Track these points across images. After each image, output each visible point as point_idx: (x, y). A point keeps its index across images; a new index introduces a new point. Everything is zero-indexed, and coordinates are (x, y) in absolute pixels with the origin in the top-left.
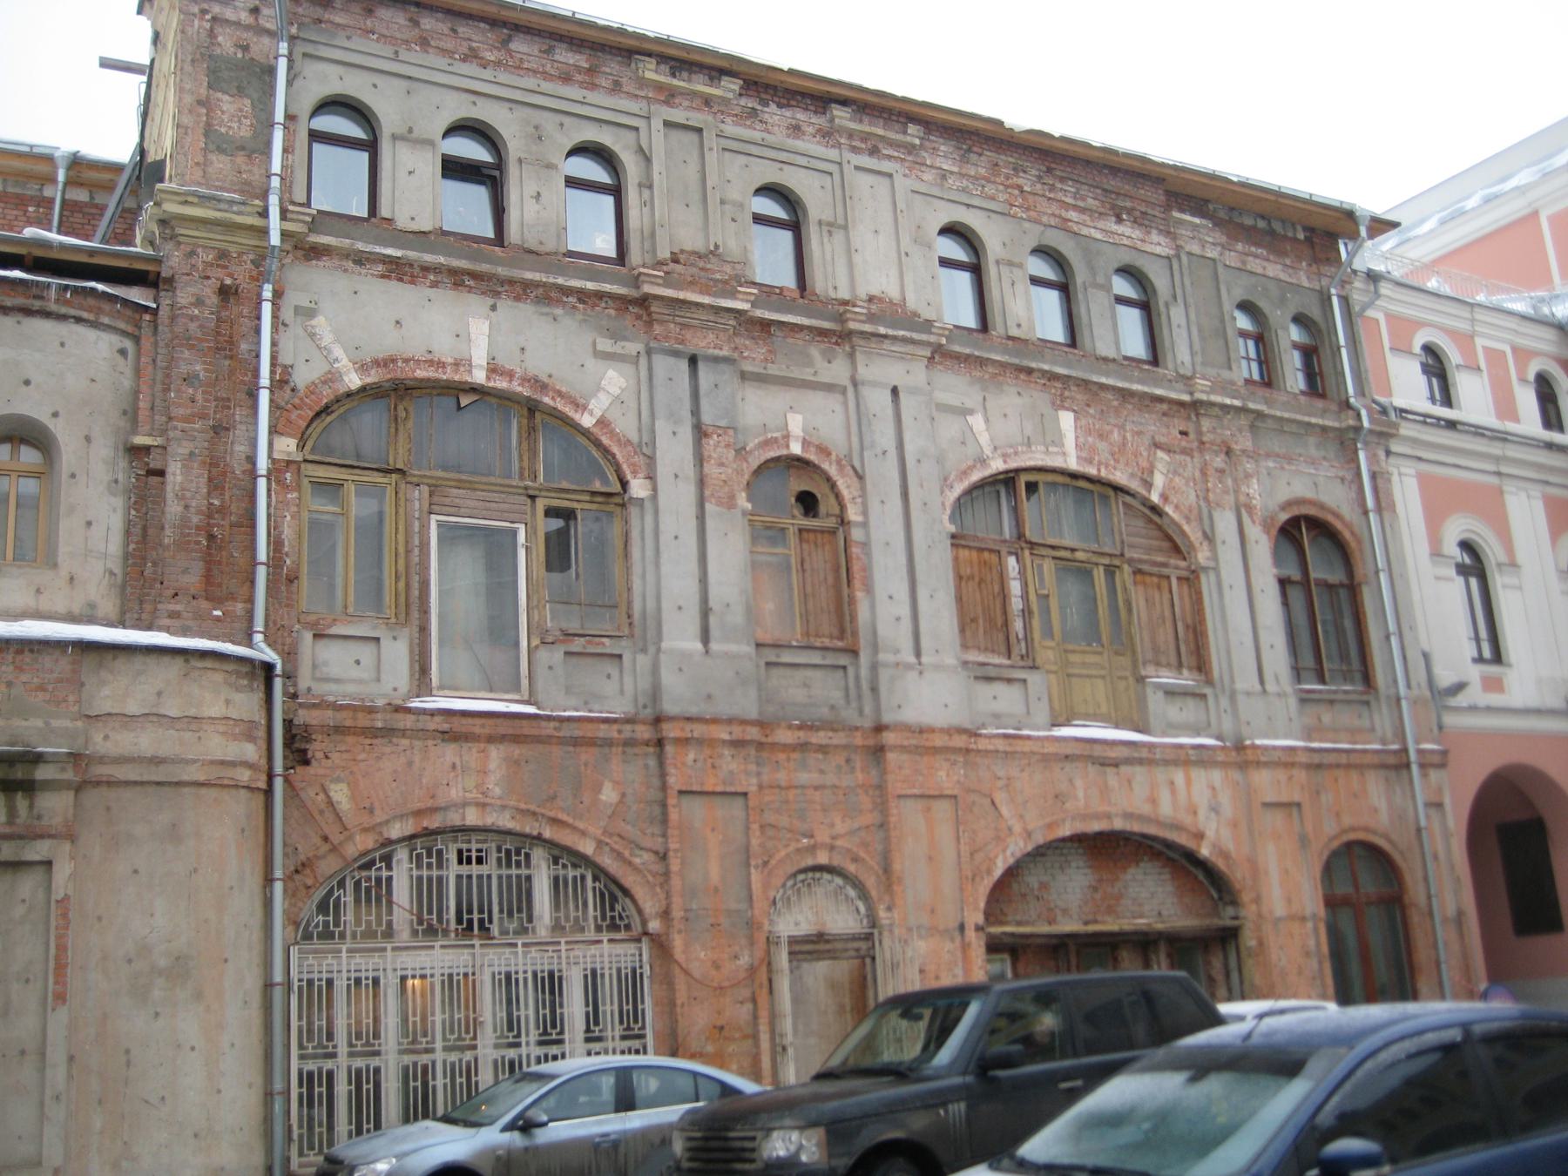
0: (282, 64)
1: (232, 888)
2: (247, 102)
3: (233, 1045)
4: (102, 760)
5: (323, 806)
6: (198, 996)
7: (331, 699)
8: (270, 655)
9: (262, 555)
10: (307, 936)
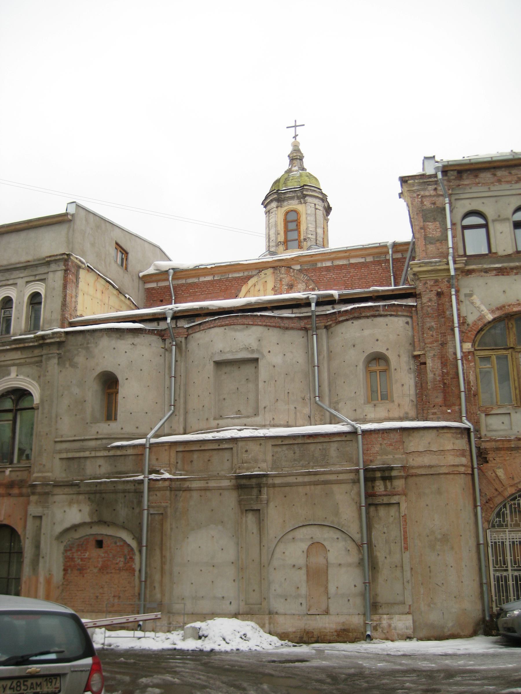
0: (447, 206)
2: (437, 223)
3: (466, 566)
4: (413, 468)
5: (495, 478)
6: (452, 548)
7: (494, 438)
8: (468, 424)
9: (462, 389)
10: (493, 526)
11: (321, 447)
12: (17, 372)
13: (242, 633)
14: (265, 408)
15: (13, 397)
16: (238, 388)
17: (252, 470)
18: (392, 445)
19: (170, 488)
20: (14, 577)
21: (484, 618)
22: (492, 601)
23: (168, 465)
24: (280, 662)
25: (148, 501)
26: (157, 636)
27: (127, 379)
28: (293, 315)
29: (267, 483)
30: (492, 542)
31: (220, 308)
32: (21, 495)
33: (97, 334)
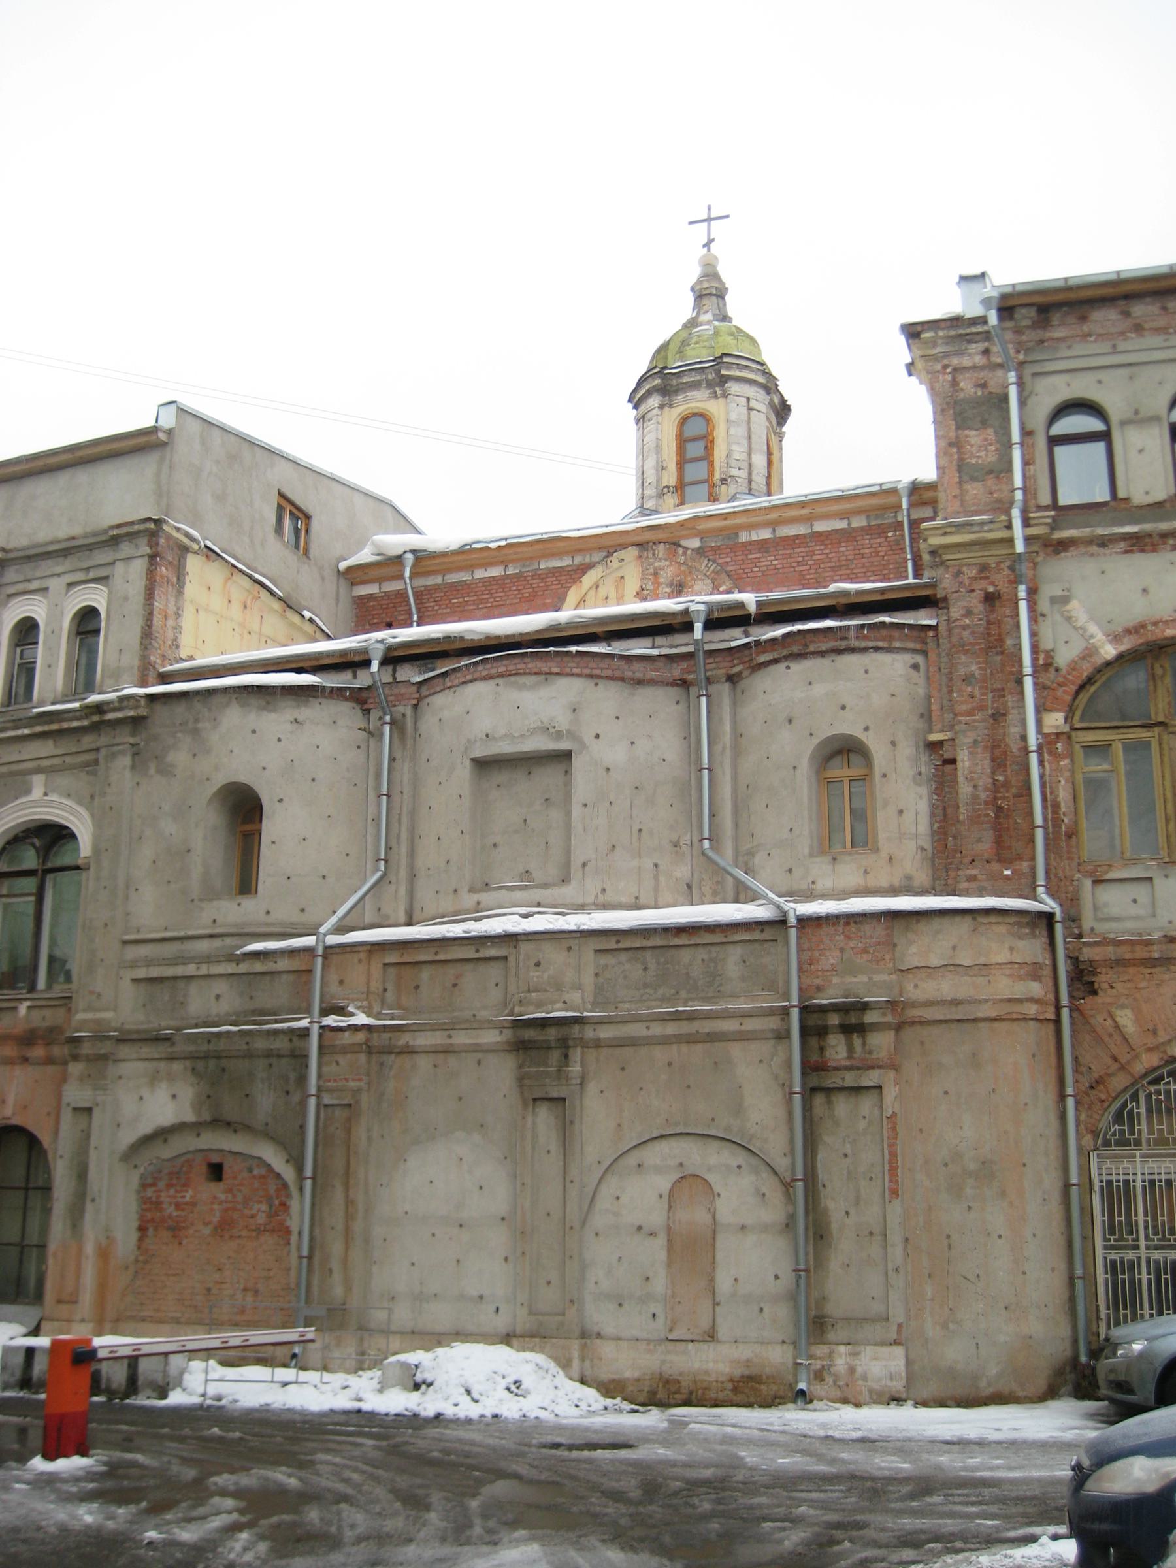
0: (1013, 392)
1: (1026, 1104)
2: (990, 431)
3: (1034, 1235)
4: (913, 1005)
5: (1111, 1030)
6: (1003, 1194)
7: (1112, 936)
8: (1048, 904)
9: (1039, 820)
10: (1107, 1143)
11: (706, 957)
12: (46, 785)
13: (511, 1379)
14: (584, 865)
15: (37, 842)
16: (525, 820)
17: (550, 1007)
18: (868, 952)
19: (369, 1047)
20: (35, 1242)
21: (1076, 1358)
22: (1098, 1318)
23: (364, 996)
24: (571, 1447)
25: (319, 1076)
26: (324, 1380)
27: (281, 801)
28: (655, 652)
29: (582, 1039)
30: (1102, 1181)
31: (488, 638)
32: (49, 1061)
33: (217, 700)
